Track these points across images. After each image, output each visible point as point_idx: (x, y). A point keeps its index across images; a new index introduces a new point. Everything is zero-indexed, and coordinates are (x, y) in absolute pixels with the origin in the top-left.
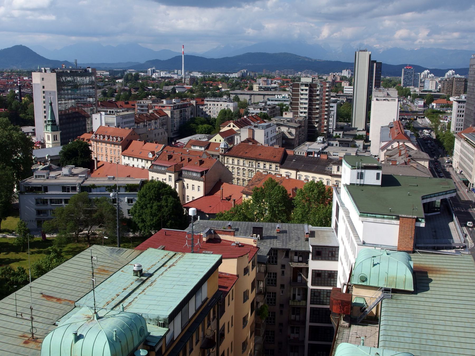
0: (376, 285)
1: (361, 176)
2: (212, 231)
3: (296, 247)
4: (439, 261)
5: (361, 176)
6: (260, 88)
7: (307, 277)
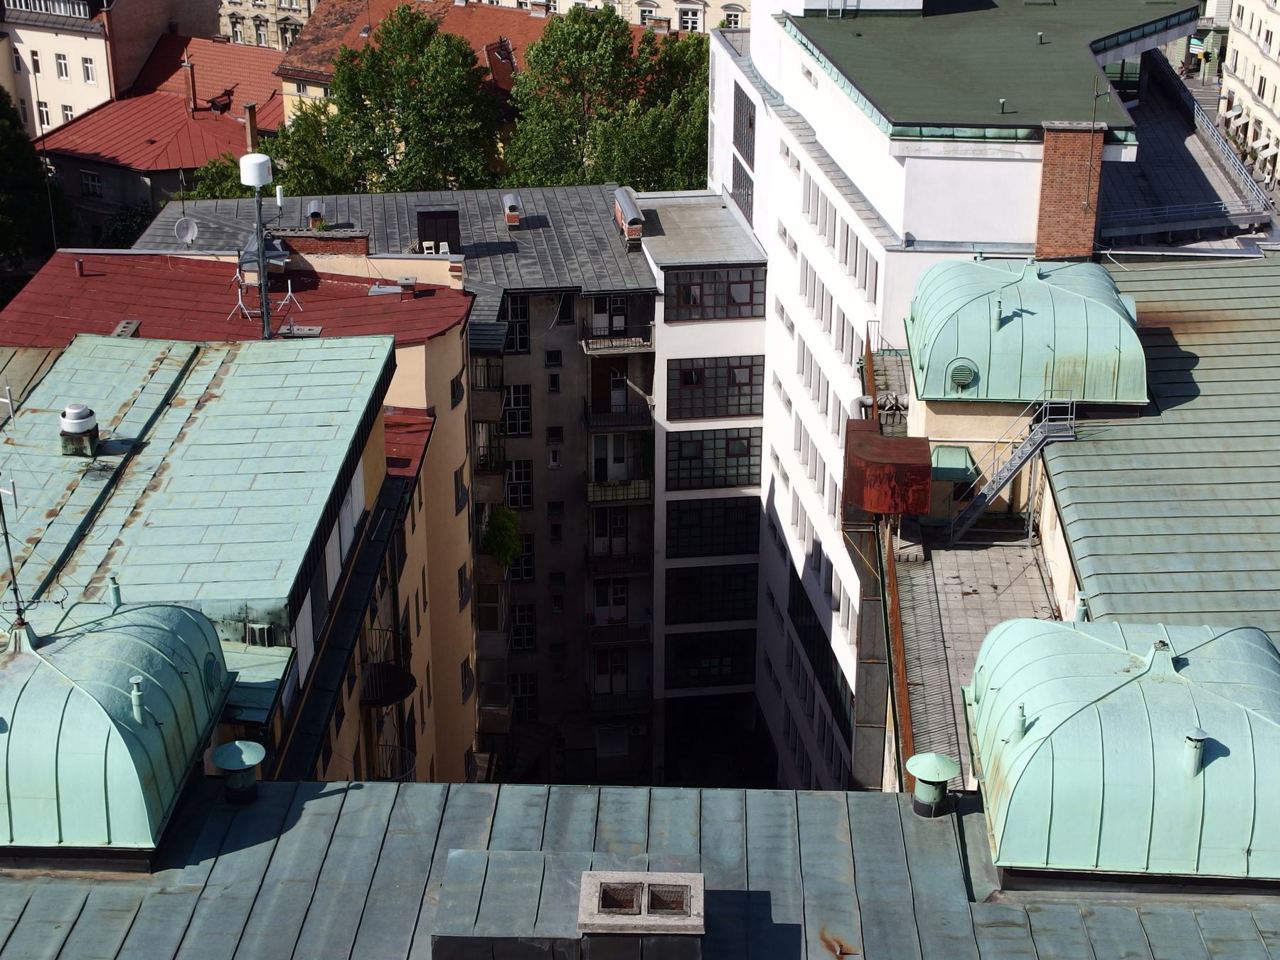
0: (1012, 396)
2: (277, 242)
3: (600, 277)
4: (1192, 284)
7: (649, 389)
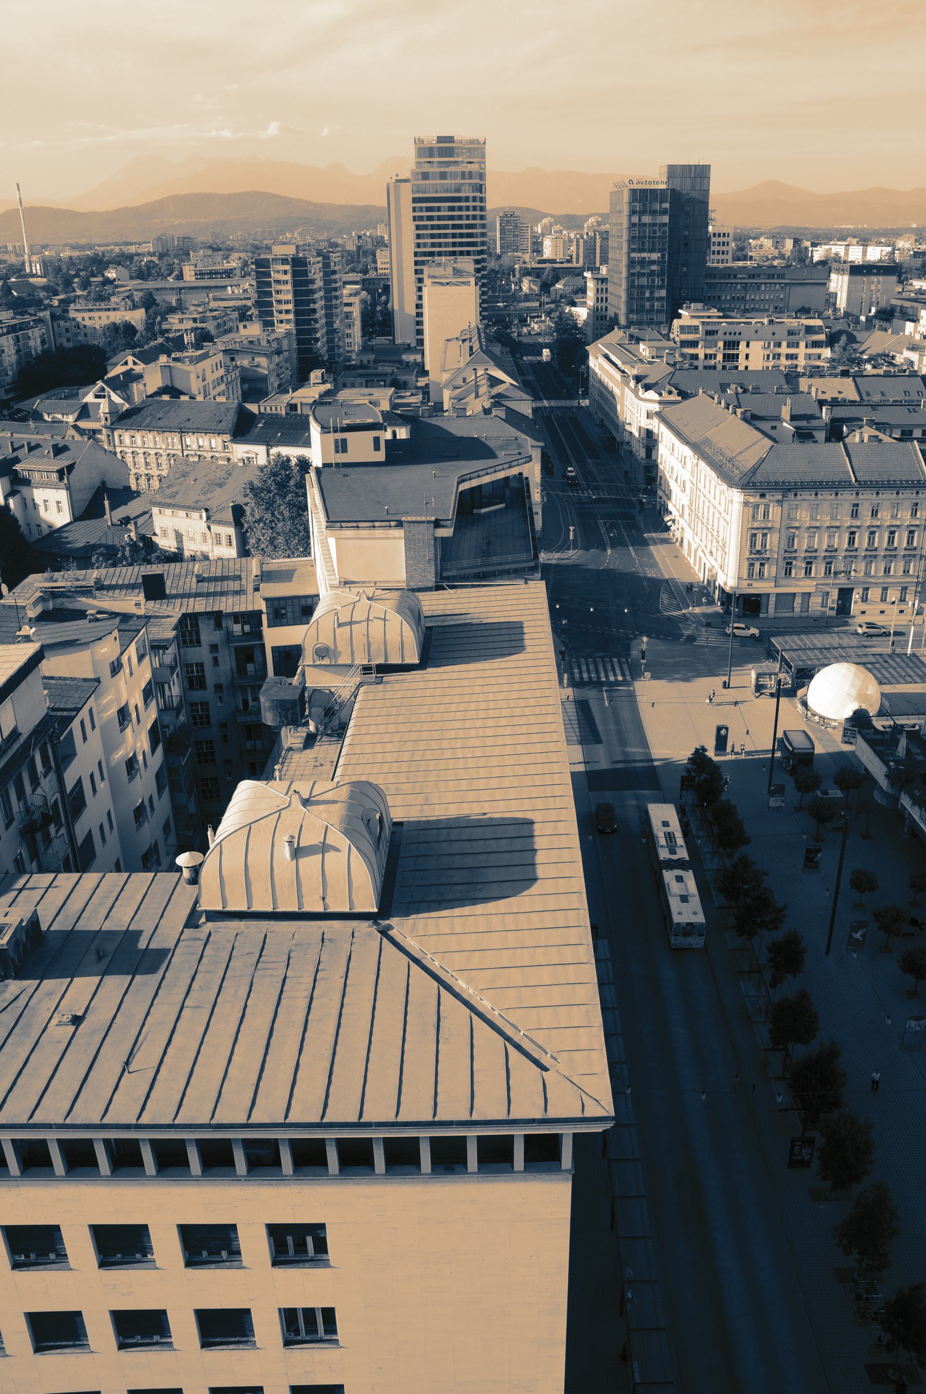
1: (342, 446)
5: (342, 446)
6: (200, 275)
